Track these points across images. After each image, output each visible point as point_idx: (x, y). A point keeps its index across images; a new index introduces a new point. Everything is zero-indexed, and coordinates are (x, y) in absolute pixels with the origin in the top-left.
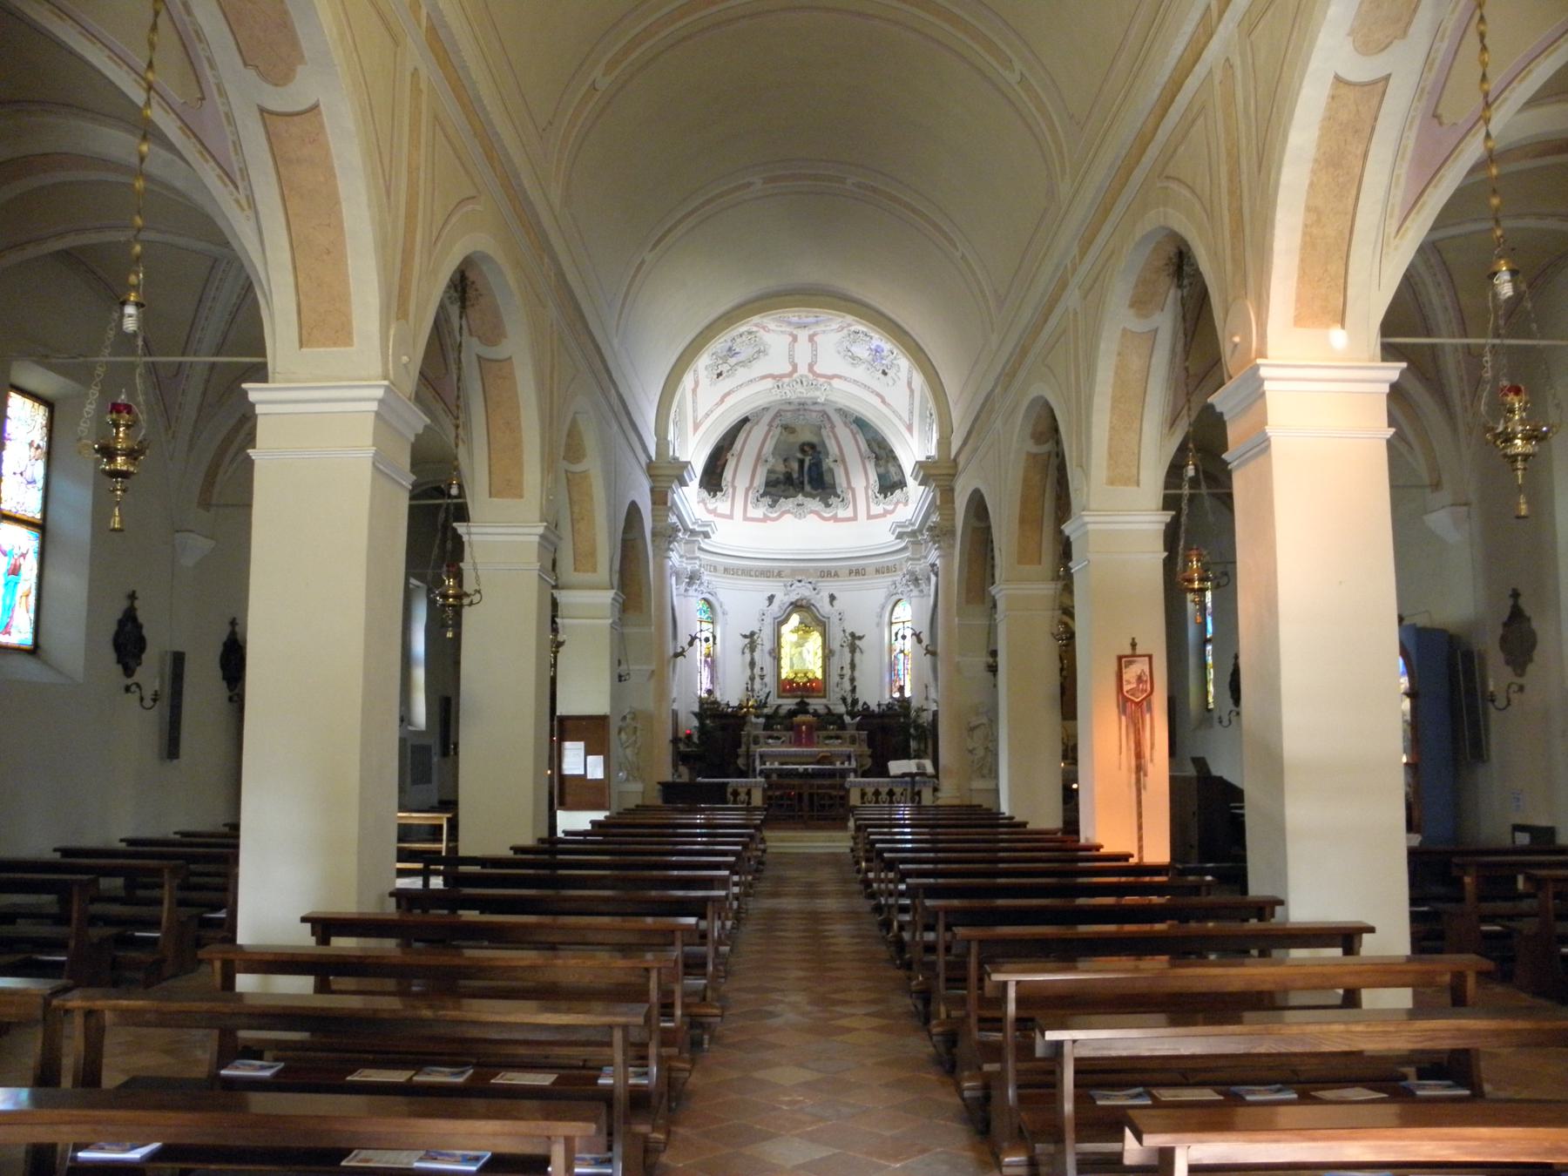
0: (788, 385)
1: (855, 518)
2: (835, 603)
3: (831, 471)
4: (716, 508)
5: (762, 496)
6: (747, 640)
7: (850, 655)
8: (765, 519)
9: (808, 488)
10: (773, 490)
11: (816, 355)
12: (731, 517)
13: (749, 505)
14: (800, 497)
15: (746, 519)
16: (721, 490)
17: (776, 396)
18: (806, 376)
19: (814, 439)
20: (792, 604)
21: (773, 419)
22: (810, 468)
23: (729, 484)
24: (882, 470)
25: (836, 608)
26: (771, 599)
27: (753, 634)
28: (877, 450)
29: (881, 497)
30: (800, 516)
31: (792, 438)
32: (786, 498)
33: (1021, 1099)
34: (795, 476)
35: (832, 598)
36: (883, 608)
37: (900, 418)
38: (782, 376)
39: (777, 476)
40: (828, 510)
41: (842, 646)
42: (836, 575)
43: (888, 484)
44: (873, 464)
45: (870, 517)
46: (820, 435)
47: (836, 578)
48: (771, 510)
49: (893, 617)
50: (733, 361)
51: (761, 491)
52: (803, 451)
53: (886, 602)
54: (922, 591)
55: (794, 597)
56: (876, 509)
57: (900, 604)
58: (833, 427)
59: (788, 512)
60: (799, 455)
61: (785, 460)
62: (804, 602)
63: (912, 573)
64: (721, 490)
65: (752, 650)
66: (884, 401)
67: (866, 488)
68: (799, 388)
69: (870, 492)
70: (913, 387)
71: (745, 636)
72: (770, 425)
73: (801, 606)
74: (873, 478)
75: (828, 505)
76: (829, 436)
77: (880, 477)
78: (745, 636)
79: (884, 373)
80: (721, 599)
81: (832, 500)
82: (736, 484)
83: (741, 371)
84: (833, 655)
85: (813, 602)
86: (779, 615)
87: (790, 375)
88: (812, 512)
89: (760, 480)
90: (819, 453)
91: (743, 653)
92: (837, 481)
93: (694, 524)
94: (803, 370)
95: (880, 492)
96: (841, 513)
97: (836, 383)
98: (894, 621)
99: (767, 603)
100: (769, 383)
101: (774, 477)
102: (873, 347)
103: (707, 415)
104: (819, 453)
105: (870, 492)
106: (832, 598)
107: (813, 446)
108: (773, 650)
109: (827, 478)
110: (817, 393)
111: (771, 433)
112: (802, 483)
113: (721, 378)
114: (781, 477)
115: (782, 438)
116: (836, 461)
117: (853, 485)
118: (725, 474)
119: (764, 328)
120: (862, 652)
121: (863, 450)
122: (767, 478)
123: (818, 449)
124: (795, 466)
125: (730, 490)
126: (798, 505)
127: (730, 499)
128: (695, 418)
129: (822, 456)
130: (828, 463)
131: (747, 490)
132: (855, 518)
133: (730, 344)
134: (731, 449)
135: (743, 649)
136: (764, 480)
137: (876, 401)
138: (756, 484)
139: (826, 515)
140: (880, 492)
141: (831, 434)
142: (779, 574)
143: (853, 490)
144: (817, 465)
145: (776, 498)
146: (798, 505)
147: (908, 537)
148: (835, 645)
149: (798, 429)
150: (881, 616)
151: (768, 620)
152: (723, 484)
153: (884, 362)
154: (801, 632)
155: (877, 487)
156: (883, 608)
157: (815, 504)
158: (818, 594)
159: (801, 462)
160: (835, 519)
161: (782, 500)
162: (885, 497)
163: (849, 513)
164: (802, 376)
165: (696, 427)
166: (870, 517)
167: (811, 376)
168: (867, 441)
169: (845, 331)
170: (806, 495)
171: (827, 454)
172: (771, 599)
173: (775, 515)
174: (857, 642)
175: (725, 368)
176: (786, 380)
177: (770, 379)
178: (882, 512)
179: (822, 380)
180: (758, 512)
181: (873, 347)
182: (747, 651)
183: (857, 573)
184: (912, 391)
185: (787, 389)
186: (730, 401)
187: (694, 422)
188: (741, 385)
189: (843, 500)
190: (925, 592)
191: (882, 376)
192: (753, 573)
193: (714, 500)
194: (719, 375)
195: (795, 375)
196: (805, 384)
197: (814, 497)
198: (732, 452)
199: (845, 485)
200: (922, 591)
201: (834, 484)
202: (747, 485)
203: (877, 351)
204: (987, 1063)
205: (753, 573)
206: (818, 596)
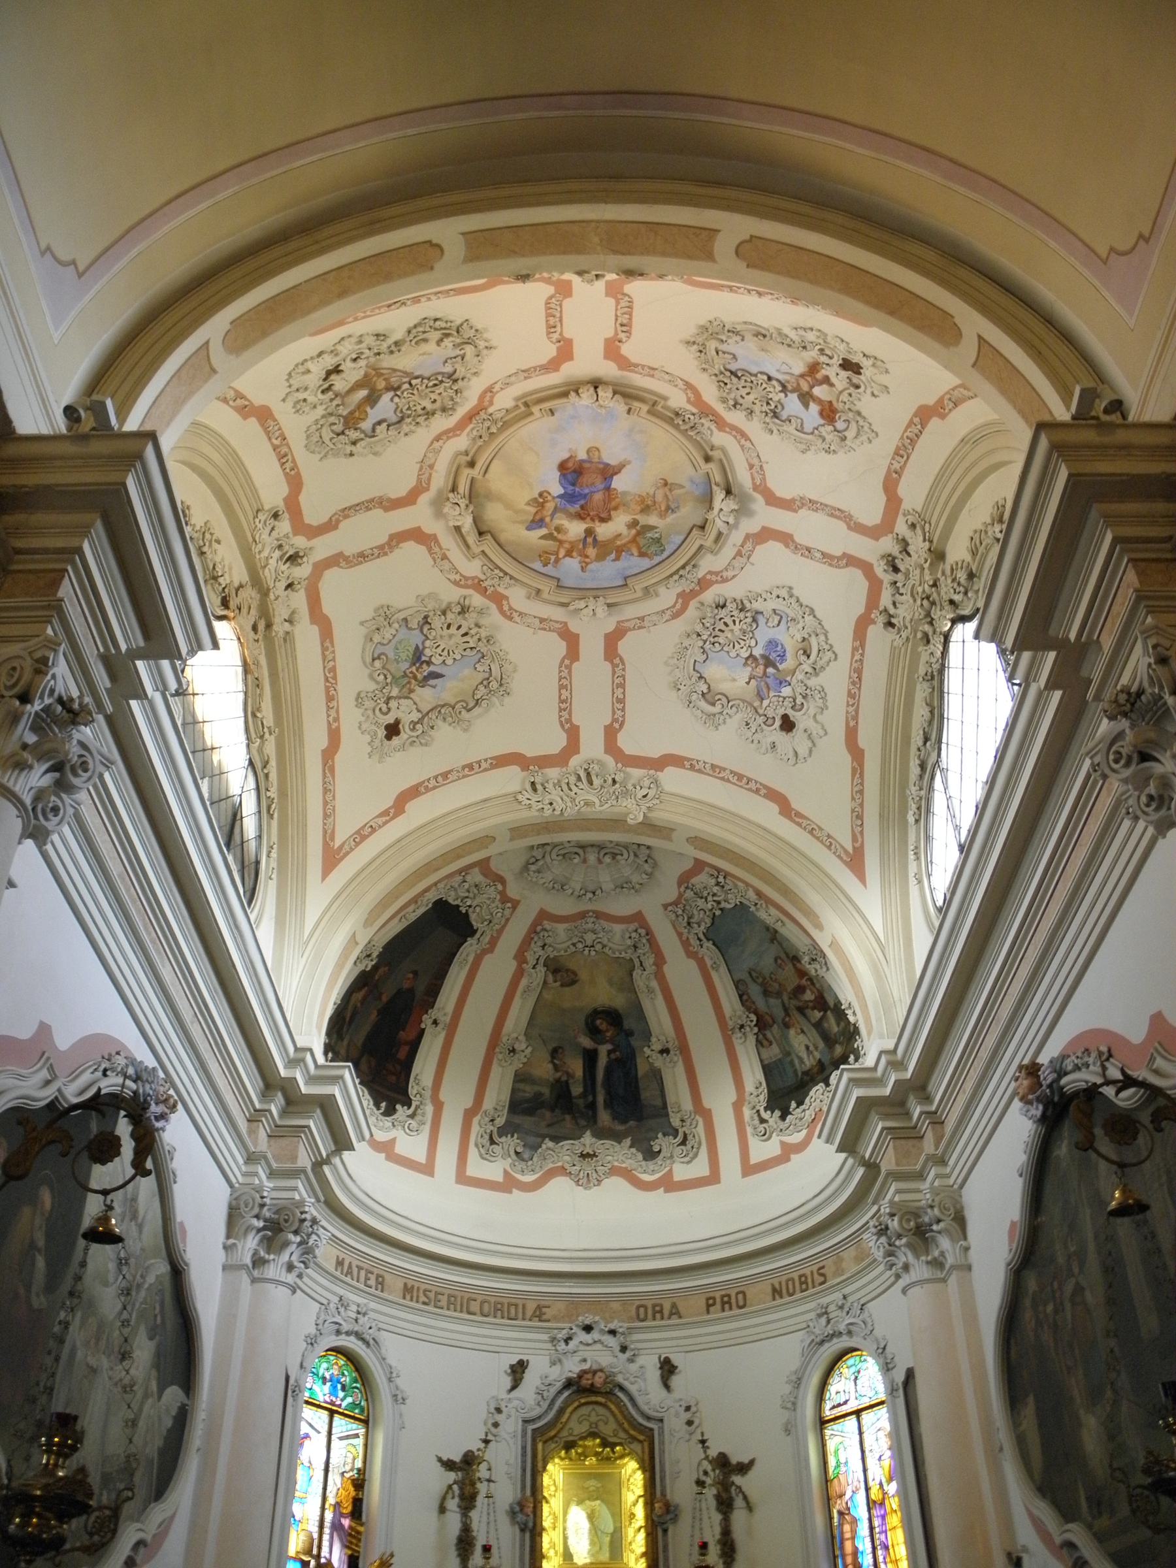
0: (558, 784)
1: (713, 1178)
2: (675, 1381)
3: (656, 1075)
4: (393, 1141)
5: (502, 1131)
6: (452, 1476)
7: (717, 1517)
8: (508, 1185)
9: (604, 1117)
10: (527, 1121)
11: (622, 701)
12: (428, 1169)
13: (473, 1153)
14: (588, 1141)
15: (462, 1178)
16: (408, 1103)
17: (531, 810)
18: (599, 762)
19: (618, 1001)
20: (569, 1384)
21: (527, 942)
22: (608, 1070)
23: (428, 1094)
24: (773, 1053)
25: (676, 1394)
26: (518, 1370)
27: (469, 1461)
28: (760, 1003)
29: (773, 1118)
30: (586, 1181)
31: (569, 998)
32: (556, 1139)
33: (60, 644)
34: (577, 1090)
35: (668, 1369)
36: (798, 1382)
37: (829, 842)
38: (544, 761)
39: (537, 1088)
40: (651, 1165)
41: (700, 1483)
42: (675, 1312)
43: (790, 1081)
44: (752, 1039)
45: (749, 1169)
46: (629, 987)
47: (675, 1320)
48: (520, 1165)
49: (828, 1405)
50: (426, 696)
51: (500, 1121)
52: (593, 1031)
53: (804, 1366)
54: (937, 1264)
55: (572, 1367)
56: (761, 1150)
57: (851, 1360)
58: (660, 960)
59: (562, 1171)
60: (586, 1042)
61: (554, 1053)
62: (599, 1380)
63: (910, 1213)
64: (408, 1103)
65: (468, 1501)
66: (786, 809)
67: (738, 1107)
68: (585, 794)
69: (747, 1113)
70: (862, 743)
71: (449, 1465)
72: (520, 957)
73: (592, 1390)
74: (753, 1077)
75: (650, 1155)
76: (650, 991)
77: (768, 1070)
78: (449, 1465)
79: (788, 725)
80: (392, 1361)
81: (662, 1143)
82: (443, 1095)
83: (444, 732)
84: (675, 1519)
85: (620, 1379)
86: (537, 1411)
87: (561, 759)
88: (614, 1171)
89: (498, 1094)
90: (629, 1034)
91: (442, 1510)
92: (671, 1099)
93: (292, 1063)
94: (592, 746)
95: (770, 1107)
96: (682, 1171)
97: (671, 778)
98: (828, 1413)
99: (507, 1382)
100: (511, 779)
101: (529, 1090)
102: (757, 652)
103: (361, 836)
104: (629, 1034)
105: (747, 1113)
106: (668, 1369)
107: (613, 1017)
108: (521, 1505)
109: (648, 1094)
110: (628, 804)
111: (524, 982)
112: (592, 1106)
113: (396, 741)
114: (546, 1091)
115: (547, 996)
116: (665, 1051)
117: (707, 1103)
118: (416, 1069)
119: (498, 599)
120: (750, 1508)
121: (727, 1010)
122: (514, 1091)
123: (628, 1024)
124: (577, 1067)
125: (429, 1109)
126: (583, 1156)
127: (427, 1129)
128: (328, 836)
129: (635, 1042)
130: (649, 1056)
131: (469, 1115)
132: (713, 1178)
133: (416, 638)
134: (432, 1005)
135: (444, 1499)
136: (506, 1097)
137: (766, 814)
138: (488, 1104)
139: (646, 1178)
140: (770, 1107)
141: (654, 984)
142: (539, 1314)
143: (707, 1115)
144: (624, 1063)
145: (532, 1140)
146: (583, 1156)
147: (886, 1116)
148: (681, 1491)
149: (583, 975)
150: (792, 1405)
151: (511, 1426)
152: (412, 1090)
153: (786, 691)
154: (591, 1461)
155: (763, 1097)
156: (798, 1382)
157: (621, 1154)
158: (631, 1360)
159: (590, 1057)
160: (669, 1184)
161: (549, 1143)
162: (783, 1118)
163: (700, 1167)
164: (590, 762)
165: (332, 858)
166: (749, 1169)
167: (610, 761)
168: (737, 984)
169: (692, 611)
170: (600, 1134)
171: (647, 1035)
172: (518, 1370)
173: (529, 1178)
174: (737, 1479)
175: (404, 712)
176: (553, 773)
177: (515, 769)
178: (777, 1151)
179: (636, 773)
180: (494, 1170)
181: (757, 652)
182: (453, 1504)
183: (726, 1303)
184: (857, 754)
185: (555, 795)
186: (419, 812)
187: (326, 845)
188: (445, 775)
189: (684, 1143)
190: (950, 1260)
191: (780, 737)
192: (475, 1306)
193: (387, 1122)
194: (393, 730)
195: (574, 761)
196: (597, 782)
197: (618, 1137)
198: (433, 1013)
199: (687, 1105)
200: (937, 1264)
201: (665, 1105)
202: (469, 1103)
203: (769, 663)
204: (57, 591)
205: (475, 1306)
206: (633, 1367)
